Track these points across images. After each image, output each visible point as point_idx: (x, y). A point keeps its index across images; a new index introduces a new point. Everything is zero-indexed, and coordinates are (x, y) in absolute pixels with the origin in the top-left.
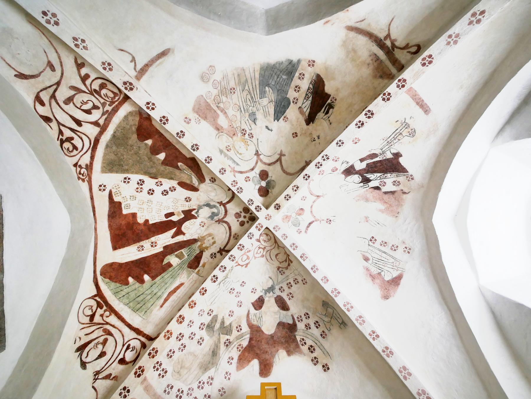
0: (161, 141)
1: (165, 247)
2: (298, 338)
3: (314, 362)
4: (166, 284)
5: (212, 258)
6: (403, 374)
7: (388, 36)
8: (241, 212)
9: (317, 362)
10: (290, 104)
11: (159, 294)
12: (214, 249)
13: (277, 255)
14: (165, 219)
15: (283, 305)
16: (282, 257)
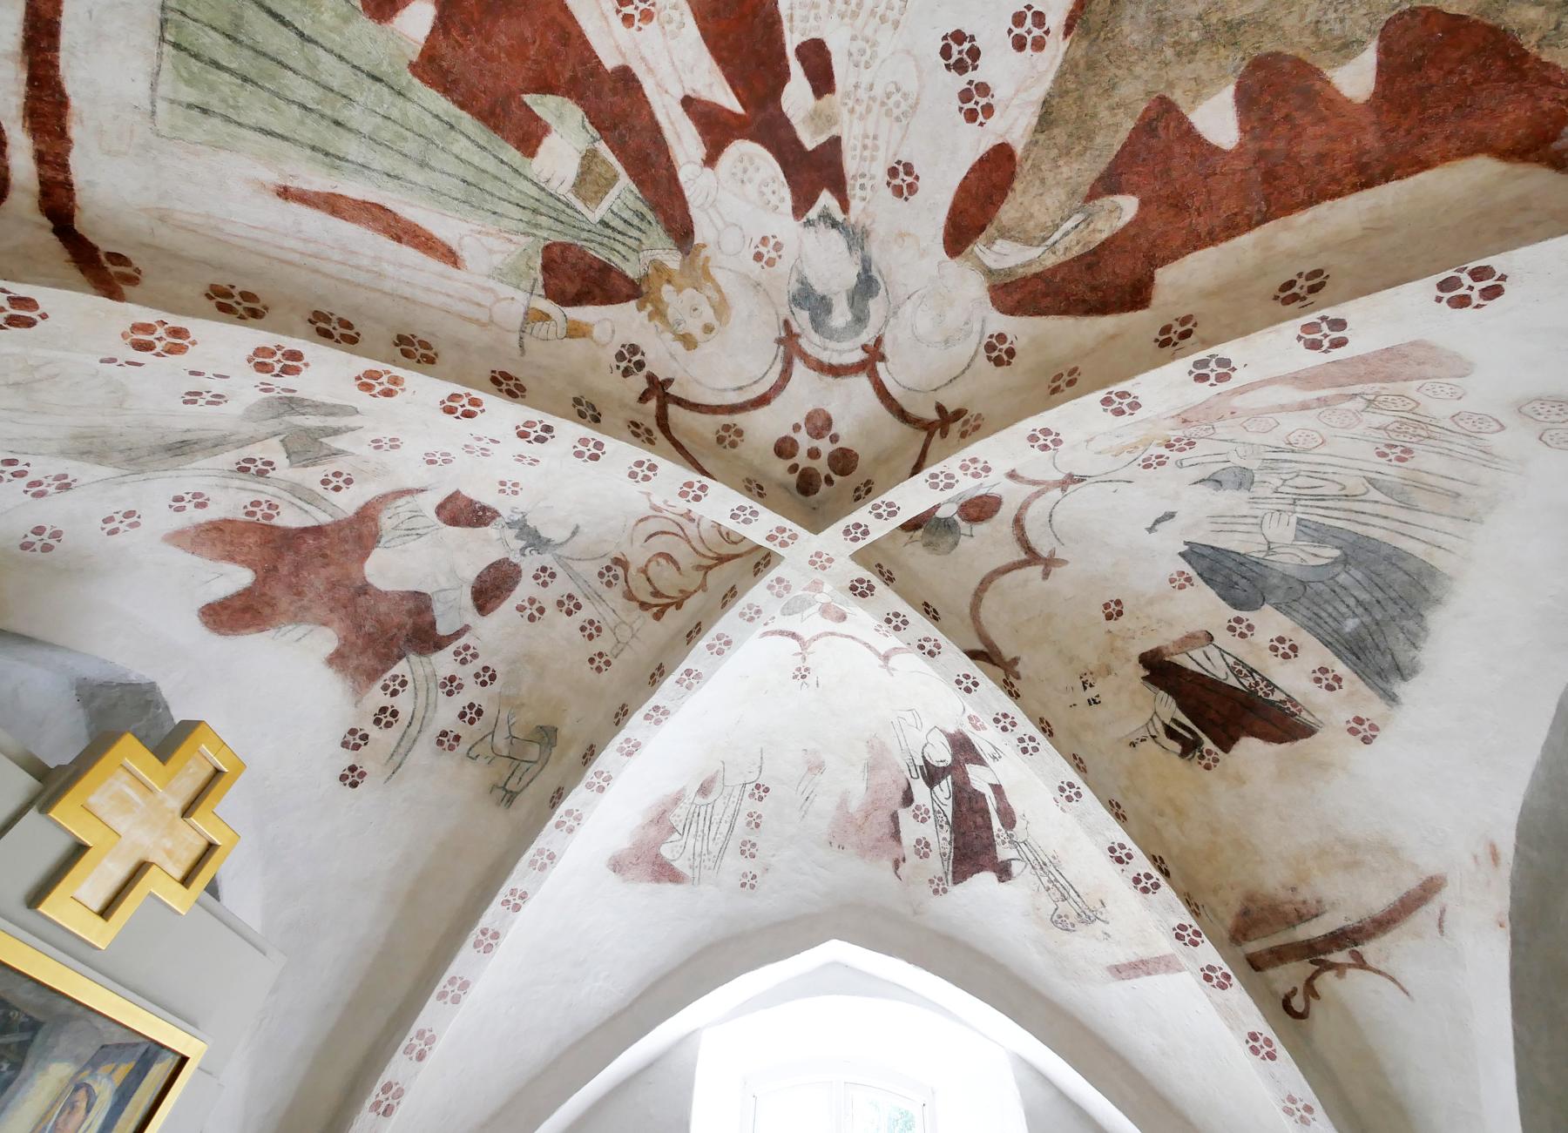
0: (1321, 158)
1: (626, 79)
2: (401, 668)
3: (350, 738)
4: (423, 164)
5: (620, 356)
6: (449, 988)
7: (1361, 963)
8: (834, 439)
9: (357, 747)
10: (1235, 606)
11: (352, 148)
12: (661, 355)
13: (669, 558)
14: (792, 41)
15: (490, 590)
16: (667, 578)
